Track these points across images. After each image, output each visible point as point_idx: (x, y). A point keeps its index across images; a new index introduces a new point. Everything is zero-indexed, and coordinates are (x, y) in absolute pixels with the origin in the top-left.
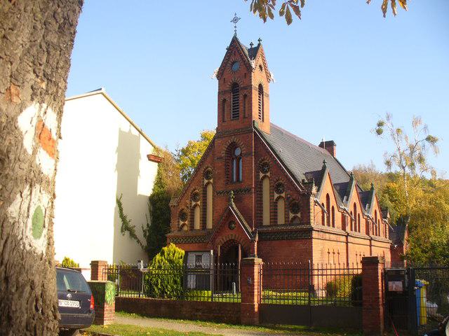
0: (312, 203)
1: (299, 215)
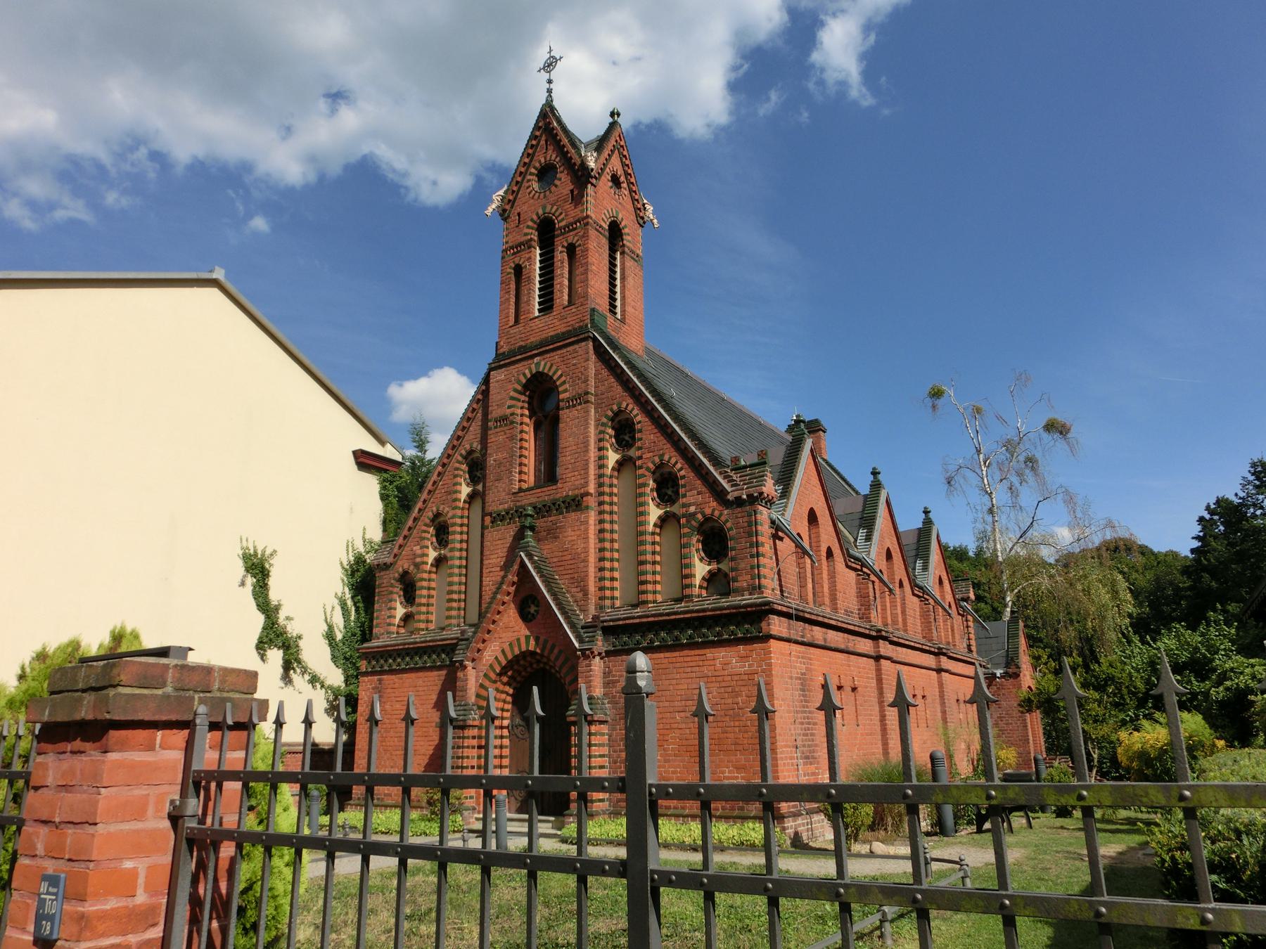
0: (765, 530)
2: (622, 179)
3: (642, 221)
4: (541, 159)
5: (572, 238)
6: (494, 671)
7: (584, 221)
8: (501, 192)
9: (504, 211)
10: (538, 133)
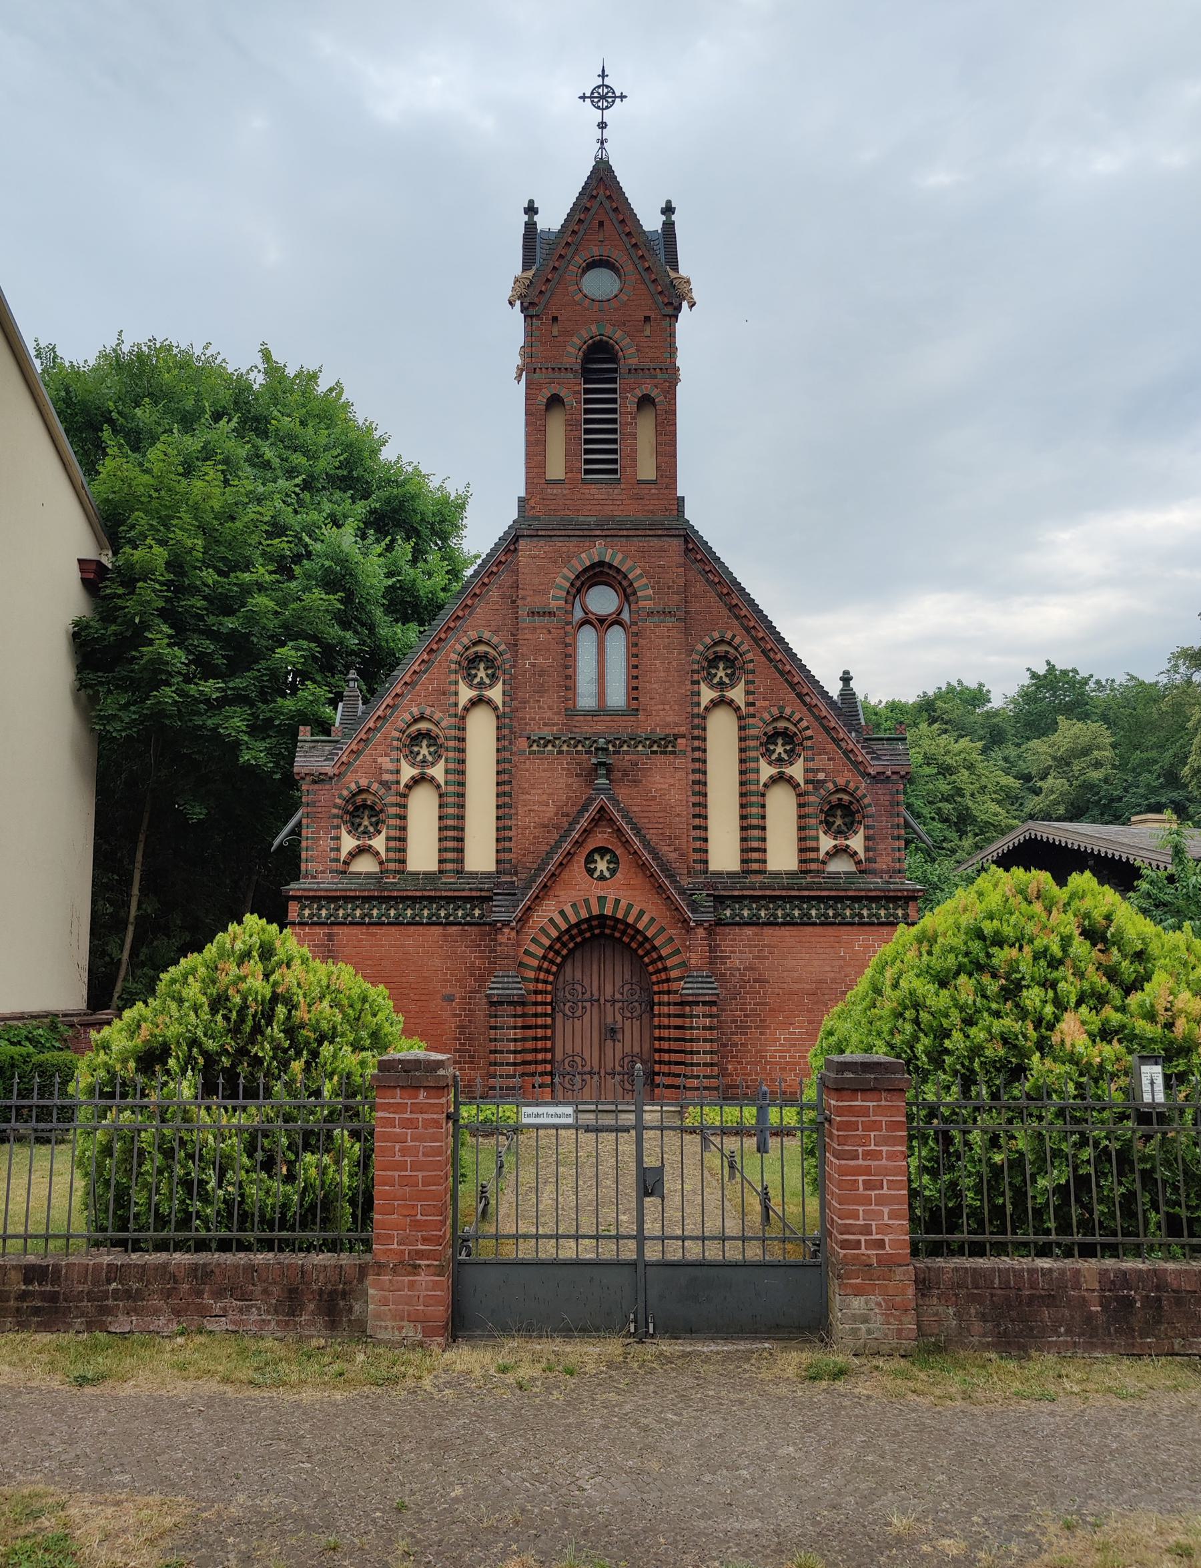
1: (856, 842)
6: (548, 936)
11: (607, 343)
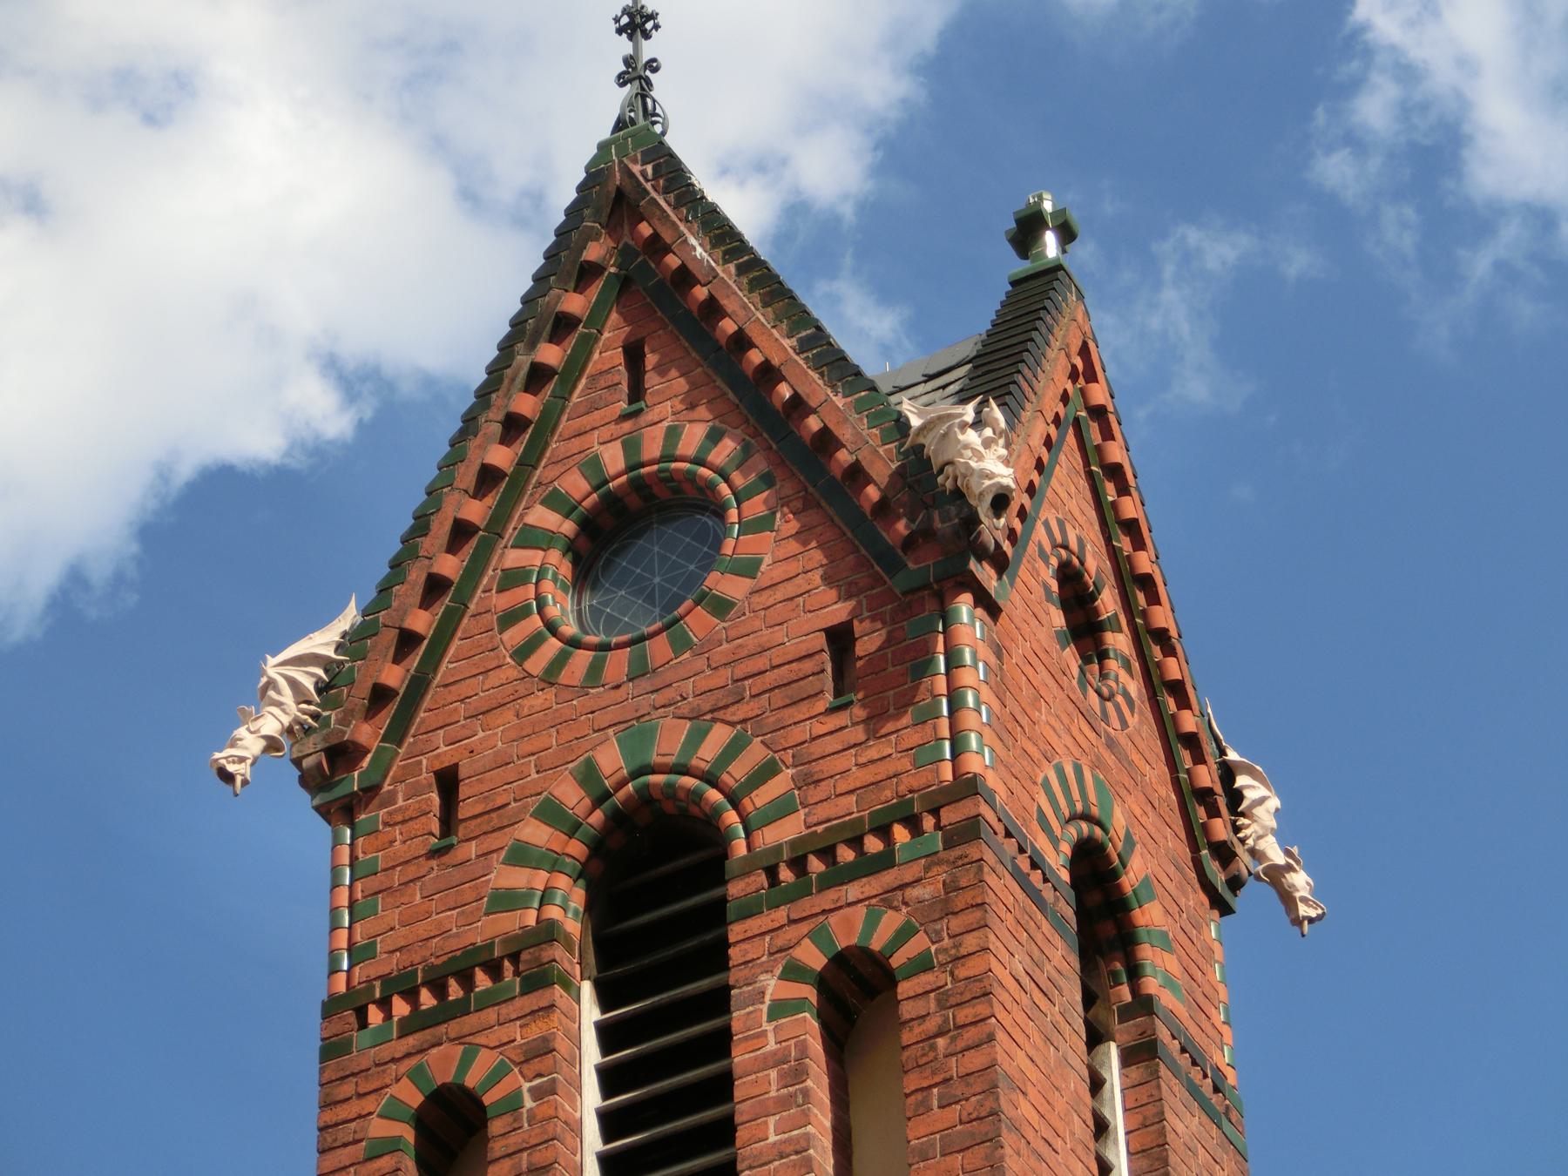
2: (1108, 602)
3: (1220, 874)
4: (598, 447)
5: (854, 918)
7: (947, 813)
8: (323, 642)
9: (342, 754)
10: (575, 304)
11: (670, 791)
